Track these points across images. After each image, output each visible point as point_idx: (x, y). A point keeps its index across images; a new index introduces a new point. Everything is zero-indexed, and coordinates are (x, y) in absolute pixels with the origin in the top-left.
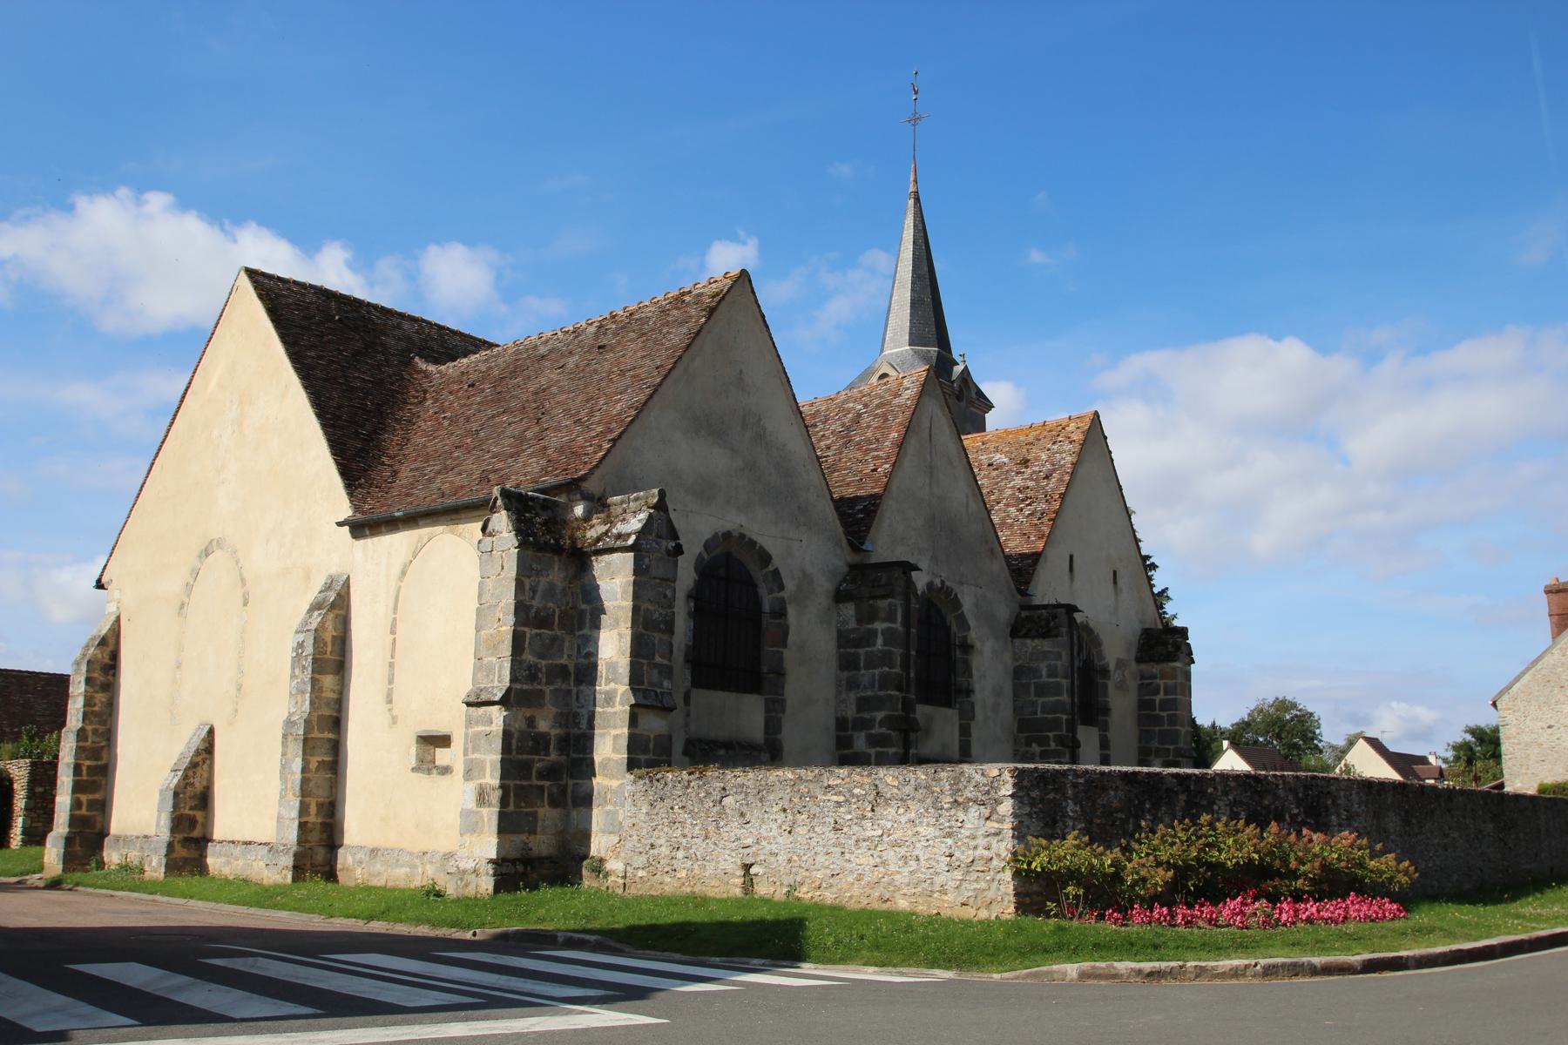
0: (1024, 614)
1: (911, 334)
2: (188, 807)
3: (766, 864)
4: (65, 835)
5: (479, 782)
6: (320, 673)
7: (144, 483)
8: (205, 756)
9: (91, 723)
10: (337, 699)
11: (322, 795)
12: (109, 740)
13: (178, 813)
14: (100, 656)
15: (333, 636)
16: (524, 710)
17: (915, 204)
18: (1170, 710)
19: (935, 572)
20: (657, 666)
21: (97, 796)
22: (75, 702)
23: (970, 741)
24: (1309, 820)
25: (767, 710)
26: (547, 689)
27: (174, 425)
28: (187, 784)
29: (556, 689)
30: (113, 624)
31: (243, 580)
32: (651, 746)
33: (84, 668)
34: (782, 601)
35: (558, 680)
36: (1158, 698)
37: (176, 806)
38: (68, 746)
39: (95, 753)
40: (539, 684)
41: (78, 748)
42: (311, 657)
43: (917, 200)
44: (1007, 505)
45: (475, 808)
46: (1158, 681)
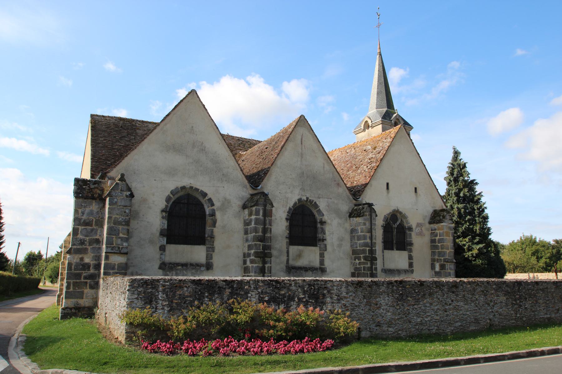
0: (356, 208)
1: (377, 105)
16: (78, 255)
17: (379, 56)
18: (441, 243)
19: (303, 194)
20: (120, 238)
23: (324, 259)
24: (311, 301)
25: (207, 251)
26: (89, 248)
29: (93, 248)
32: (116, 267)
34: (214, 210)
35: (95, 244)
36: (437, 238)
40: (86, 245)
43: (380, 55)
44: (364, 165)
46: (437, 231)
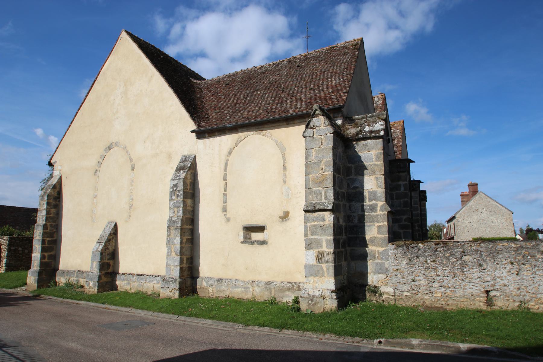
2: (106, 259)
3: (501, 291)
4: (38, 271)
5: (317, 250)
6: (186, 199)
7: (73, 121)
8: (113, 236)
9: (49, 222)
10: (193, 210)
11: (188, 254)
12: (57, 229)
13: (102, 262)
14: (53, 193)
15: (190, 182)
21: (52, 253)
22: (41, 213)
27: (88, 97)
28: (106, 248)
30: (58, 180)
31: (131, 160)
33: (46, 198)
37: (102, 259)
38: (38, 232)
39: (51, 235)
41: (44, 233)
42: (182, 191)
45: (315, 264)
